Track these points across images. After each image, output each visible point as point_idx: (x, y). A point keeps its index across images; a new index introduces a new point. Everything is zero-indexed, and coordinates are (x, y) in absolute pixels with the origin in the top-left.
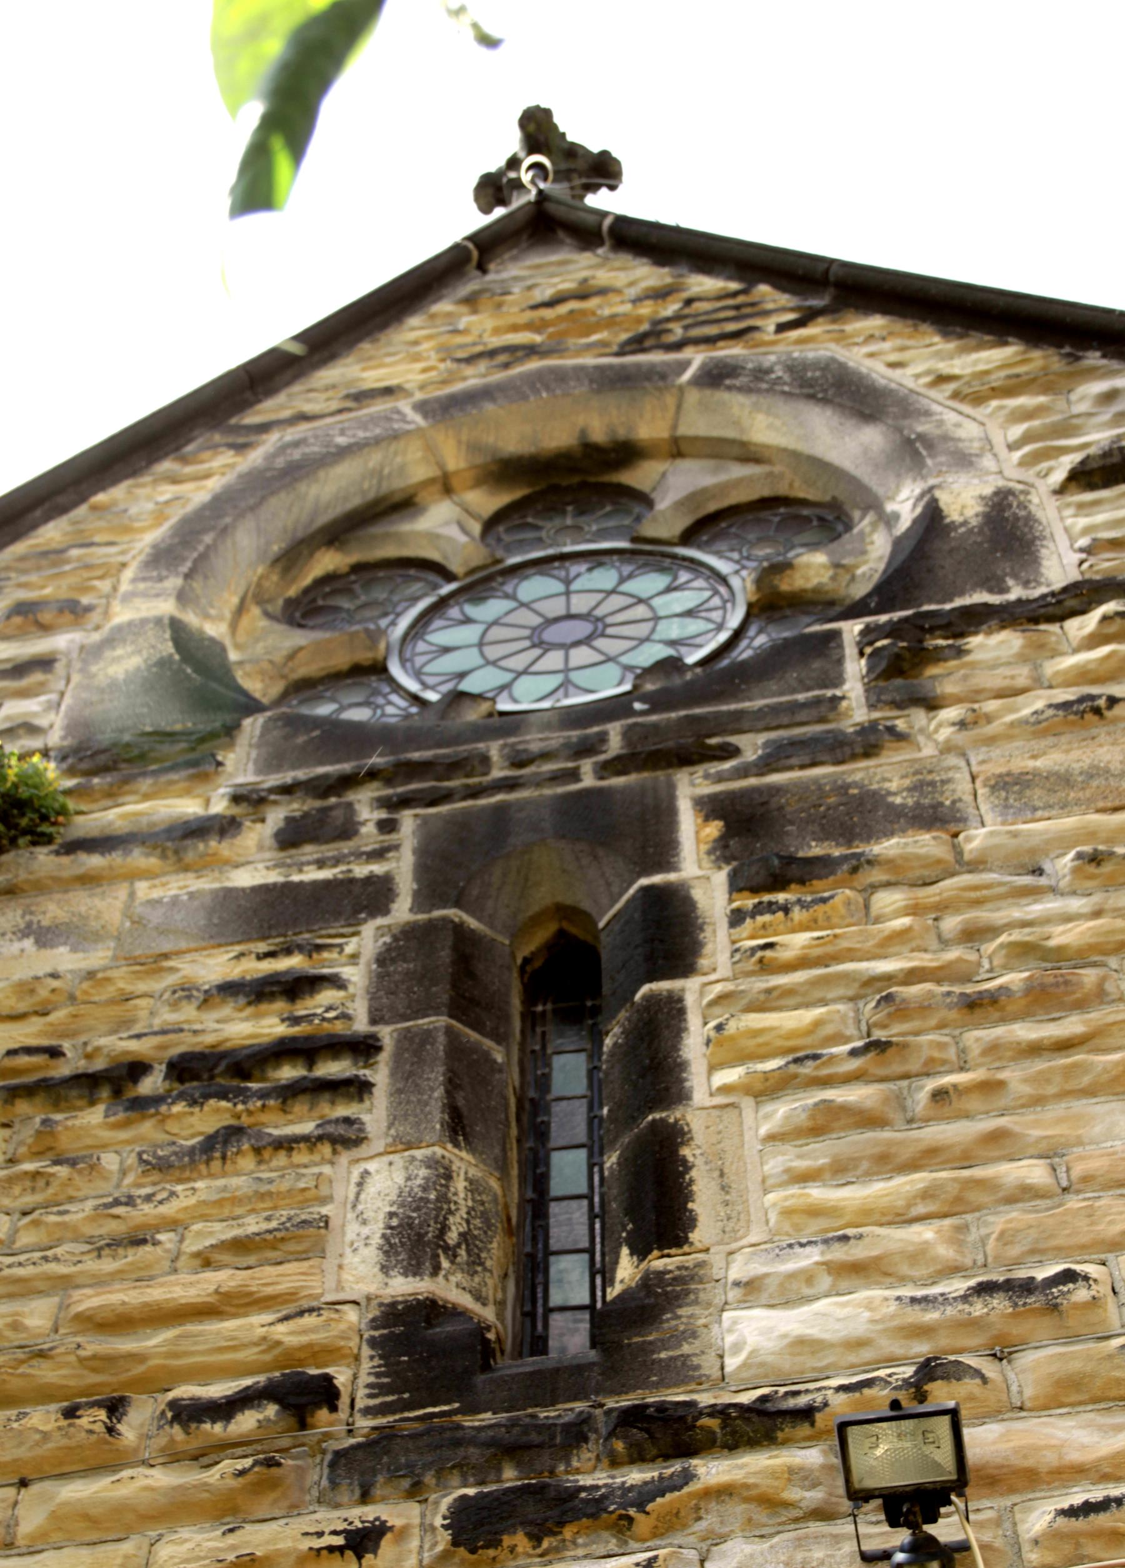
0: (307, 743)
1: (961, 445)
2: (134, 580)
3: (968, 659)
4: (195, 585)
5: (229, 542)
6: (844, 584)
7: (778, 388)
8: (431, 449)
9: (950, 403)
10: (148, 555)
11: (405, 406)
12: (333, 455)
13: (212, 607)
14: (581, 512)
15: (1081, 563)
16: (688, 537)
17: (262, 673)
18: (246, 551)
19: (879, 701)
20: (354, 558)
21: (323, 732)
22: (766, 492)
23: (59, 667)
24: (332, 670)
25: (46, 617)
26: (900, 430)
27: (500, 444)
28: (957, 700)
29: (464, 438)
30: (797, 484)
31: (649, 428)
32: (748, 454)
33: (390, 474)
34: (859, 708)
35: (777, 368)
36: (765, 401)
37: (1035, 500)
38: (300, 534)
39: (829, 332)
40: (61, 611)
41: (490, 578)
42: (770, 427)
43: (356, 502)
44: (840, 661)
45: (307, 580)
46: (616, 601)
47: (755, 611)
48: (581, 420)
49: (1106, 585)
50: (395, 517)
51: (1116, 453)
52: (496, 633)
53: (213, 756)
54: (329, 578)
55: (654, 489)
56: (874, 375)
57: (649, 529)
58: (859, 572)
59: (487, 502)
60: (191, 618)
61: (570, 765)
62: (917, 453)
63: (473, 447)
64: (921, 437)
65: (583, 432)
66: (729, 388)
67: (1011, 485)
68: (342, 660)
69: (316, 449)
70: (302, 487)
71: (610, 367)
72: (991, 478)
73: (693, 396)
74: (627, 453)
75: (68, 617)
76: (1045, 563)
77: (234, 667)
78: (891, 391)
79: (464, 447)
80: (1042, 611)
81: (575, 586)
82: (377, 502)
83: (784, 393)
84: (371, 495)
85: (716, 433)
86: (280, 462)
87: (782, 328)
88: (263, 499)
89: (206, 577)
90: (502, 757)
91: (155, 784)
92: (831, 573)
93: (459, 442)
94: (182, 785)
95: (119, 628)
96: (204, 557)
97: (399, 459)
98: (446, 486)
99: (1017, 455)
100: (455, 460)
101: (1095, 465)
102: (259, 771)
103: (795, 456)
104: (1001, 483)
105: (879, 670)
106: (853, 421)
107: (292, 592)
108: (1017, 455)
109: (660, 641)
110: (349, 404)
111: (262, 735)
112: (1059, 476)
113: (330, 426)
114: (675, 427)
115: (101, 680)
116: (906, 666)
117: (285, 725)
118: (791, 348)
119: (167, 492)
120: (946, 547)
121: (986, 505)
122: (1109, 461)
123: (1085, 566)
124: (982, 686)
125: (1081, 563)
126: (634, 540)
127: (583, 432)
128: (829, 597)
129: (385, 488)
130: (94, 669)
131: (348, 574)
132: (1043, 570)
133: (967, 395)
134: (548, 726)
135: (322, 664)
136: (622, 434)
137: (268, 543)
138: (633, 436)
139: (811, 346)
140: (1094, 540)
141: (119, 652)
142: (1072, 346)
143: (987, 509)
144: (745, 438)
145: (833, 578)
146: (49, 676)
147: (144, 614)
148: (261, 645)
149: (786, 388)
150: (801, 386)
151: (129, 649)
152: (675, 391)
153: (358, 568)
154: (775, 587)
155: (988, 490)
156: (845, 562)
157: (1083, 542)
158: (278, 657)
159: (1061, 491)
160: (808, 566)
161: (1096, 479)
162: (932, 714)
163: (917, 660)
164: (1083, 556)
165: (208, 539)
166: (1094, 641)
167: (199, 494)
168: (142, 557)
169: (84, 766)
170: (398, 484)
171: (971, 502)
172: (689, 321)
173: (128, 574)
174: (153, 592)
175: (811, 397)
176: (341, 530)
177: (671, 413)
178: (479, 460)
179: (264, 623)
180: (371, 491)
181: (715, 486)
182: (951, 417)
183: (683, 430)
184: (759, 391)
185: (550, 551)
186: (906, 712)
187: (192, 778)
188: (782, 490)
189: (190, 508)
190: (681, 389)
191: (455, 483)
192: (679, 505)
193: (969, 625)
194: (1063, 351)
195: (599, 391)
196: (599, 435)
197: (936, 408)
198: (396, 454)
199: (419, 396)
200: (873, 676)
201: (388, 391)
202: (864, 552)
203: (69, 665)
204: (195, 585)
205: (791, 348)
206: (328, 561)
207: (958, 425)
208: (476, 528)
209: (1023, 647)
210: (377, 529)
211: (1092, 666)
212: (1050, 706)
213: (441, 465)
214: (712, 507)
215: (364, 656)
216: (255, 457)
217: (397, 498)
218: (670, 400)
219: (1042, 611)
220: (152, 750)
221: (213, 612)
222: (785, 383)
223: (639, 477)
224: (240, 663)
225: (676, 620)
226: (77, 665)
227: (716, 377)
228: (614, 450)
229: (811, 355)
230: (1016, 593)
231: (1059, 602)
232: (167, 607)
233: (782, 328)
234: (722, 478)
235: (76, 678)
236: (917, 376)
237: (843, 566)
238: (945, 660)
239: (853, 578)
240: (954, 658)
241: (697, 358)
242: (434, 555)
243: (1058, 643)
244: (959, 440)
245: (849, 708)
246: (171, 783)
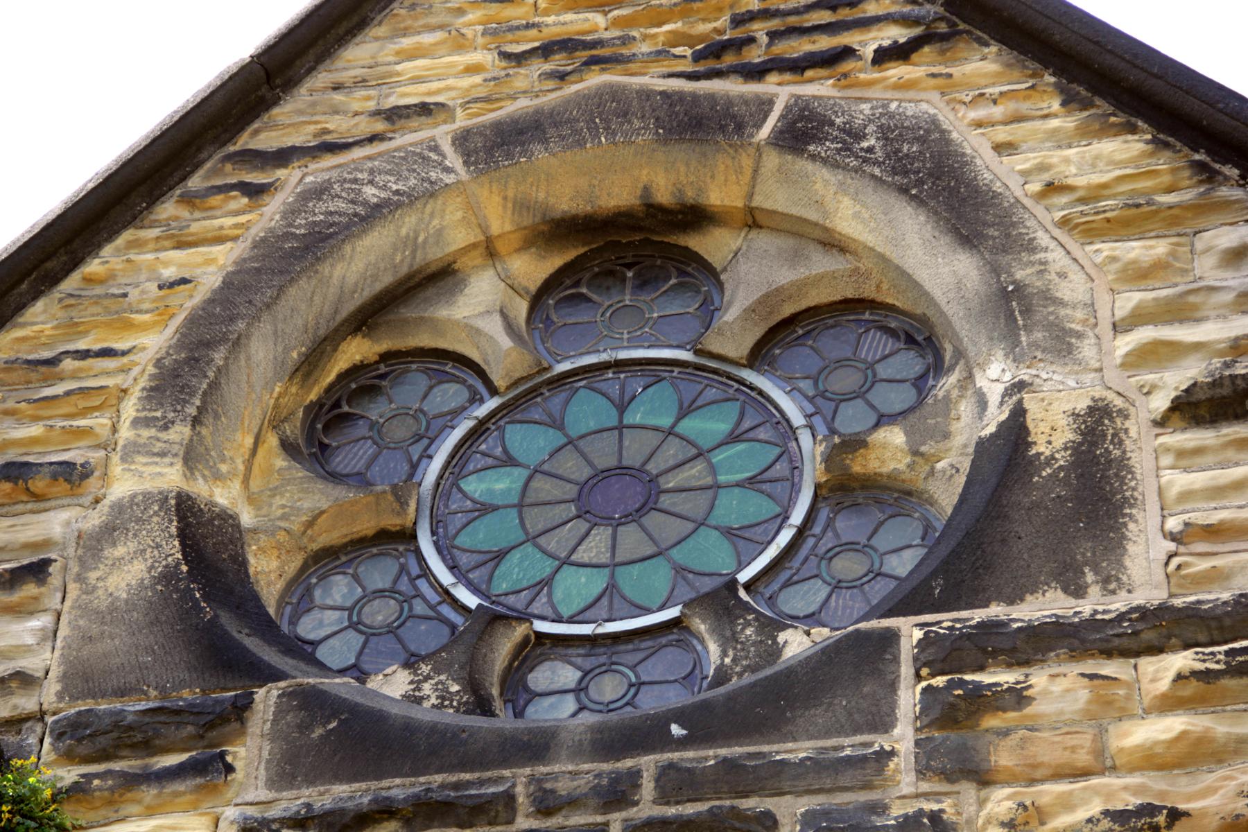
0: (324, 738)
1: (1063, 312)
2: (136, 422)
3: (1028, 710)
4: (204, 431)
5: (242, 357)
6: (923, 476)
7: (868, 169)
8: (472, 208)
9: (1057, 232)
10: (153, 377)
11: (442, 133)
12: (363, 219)
13: (223, 461)
14: (643, 283)
15: (1171, 556)
16: (759, 356)
17: (279, 546)
18: (261, 374)
19: (928, 768)
20: (384, 346)
21: (341, 722)
22: (850, 294)
23: (55, 580)
24: (355, 536)
25: (38, 484)
26: (996, 270)
27: (552, 200)
28: (1011, 779)
29: (510, 193)
30: (885, 287)
31: (721, 194)
32: (833, 243)
33: (425, 241)
34: (907, 771)
35: (871, 128)
36: (854, 182)
37: (1133, 433)
38: (322, 332)
39: (933, 75)
40: (55, 477)
41: (534, 392)
42: (856, 215)
43: (387, 280)
44: (893, 687)
45: (332, 377)
46: (673, 451)
47: (824, 492)
48: (644, 176)
49: (1188, 617)
50: (431, 291)
51: (1227, 382)
52: (539, 483)
53: (222, 755)
54: (356, 370)
55: (725, 269)
56: (978, 162)
57: (714, 344)
58: (939, 466)
59: (533, 269)
60: (200, 488)
61: (599, 819)
62: (1011, 317)
63: (521, 206)
64: (1020, 288)
65: (646, 190)
66: (813, 157)
67: (1110, 396)
68: (366, 525)
69: (341, 205)
70: (325, 269)
71: (680, 96)
72: (1089, 378)
73: (772, 160)
74: (695, 217)
75: (63, 486)
76: (1131, 548)
77: (247, 538)
78: (996, 195)
79: (510, 205)
80: (1117, 642)
81: (635, 416)
82: (409, 277)
83: (873, 176)
84: (404, 270)
85: (795, 211)
86: (300, 226)
87: (883, 56)
88: (281, 289)
89: (217, 417)
90: (528, 796)
91: (159, 795)
92: (908, 460)
93: (505, 198)
94: (189, 797)
95: (119, 508)
96: (214, 386)
97: (435, 222)
98: (490, 250)
99: (1125, 344)
100: (500, 222)
101: (1201, 395)
102: (272, 784)
103: (882, 258)
104: (1099, 392)
105: (932, 717)
106: (948, 239)
107: (313, 396)
108: (1125, 344)
109: (716, 528)
110: (380, 126)
111: (275, 721)
112: (1160, 402)
113: (357, 166)
114: (750, 196)
115: (101, 600)
116: (961, 715)
117: (300, 708)
118: (888, 95)
119: (173, 263)
120: (1026, 501)
121: (1078, 430)
122: (1219, 392)
123: (1175, 561)
124: (1040, 759)
125: (1171, 556)
126: (698, 352)
127: (646, 190)
128: (906, 486)
129: (419, 261)
130: (93, 576)
131: (376, 362)
132: (1127, 562)
133: (1077, 225)
134: (578, 753)
135: (345, 531)
136: (690, 196)
137: (287, 350)
138: (702, 201)
139: (911, 94)
140: (1187, 524)
141: (120, 551)
142: (1208, 153)
143: (1079, 438)
144: (828, 224)
145: (910, 466)
146: (43, 589)
147: (149, 486)
148: (278, 501)
149: (877, 171)
150: (894, 172)
151: (132, 546)
152: (752, 151)
153: (385, 357)
154: (848, 468)
155: (1082, 405)
156: (923, 449)
157: (1173, 524)
158: (296, 525)
159: (1161, 423)
160: (884, 446)
161: (1203, 411)
162: (983, 793)
163: (973, 708)
164: (1172, 546)
165: (218, 356)
166: (1168, 704)
167: (211, 266)
168: (143, 382)
169: (83, 750)
170: (434, 255)
171: (1062, 421)
172: (775, 24)
173: (130, 409)
174: (159, 446)
175: (903, 190)
176: (369, 316)
177: (748, 172)
178: (527, 221)
179: (281, 462)
180: (403, 265)
181: (792, 284)
182: (1056, 257)
183: (758, 201)
184: (846, 168)
185: (604, 357)
186: (955, 788)
187: (199, 788)
188: (868, 292)
189: (201, 172)
190: (758, 147)
191: (501, 247)
192: (751, 310)
193: (1036, 651)
194: (1197, 157)
195: (665, 141)
196: (664, 196)
197: (1043, 239)
198: (432, 215)
199: (462, 121)
200: (926, 720)
201: (424, 109)
202: (947, 436)
203: (65, 568)
204: (204, 431)
205: (888, 95)
206: (356, 351)
207: (1062, 275)
208: (521, 308)
209: (1089, 702)
210: (408, 312)
211: (1159, 750)
212: (1106, 813)
213: (484, 228)
214: (788, 310)
215: (392, 522)
216: (271, 211)
217: (433, 268)
218: (747, 162)
219: (1117, 642)
220: (157, 735)
221: (224, 468)
222: (876, 163)
223: (713, 245)
224: (254, 531)
225: (737, 490)
226: (75, 569)
227: (802, 132)
228: (680, 212)
229: (910, 109)
230: (1088, 606)
231: (1136, 633)
232: (171, 477)
233: (883, 56)
234: (801, 272)
235: (73, 590)
236: (1025, 174)
237: (922, 455)
238: (1005, 710)
239: (932, 472)
240: (1014, 710)
241: (781, 92)
242: (475, 355)
243: (1128, 698)
244: (1061, 303)
245: (897, 771)
246: (177, 794)
